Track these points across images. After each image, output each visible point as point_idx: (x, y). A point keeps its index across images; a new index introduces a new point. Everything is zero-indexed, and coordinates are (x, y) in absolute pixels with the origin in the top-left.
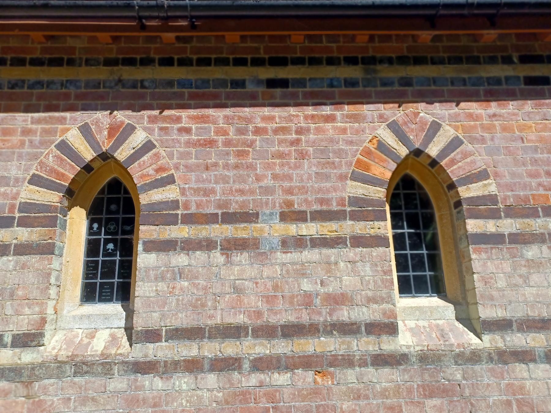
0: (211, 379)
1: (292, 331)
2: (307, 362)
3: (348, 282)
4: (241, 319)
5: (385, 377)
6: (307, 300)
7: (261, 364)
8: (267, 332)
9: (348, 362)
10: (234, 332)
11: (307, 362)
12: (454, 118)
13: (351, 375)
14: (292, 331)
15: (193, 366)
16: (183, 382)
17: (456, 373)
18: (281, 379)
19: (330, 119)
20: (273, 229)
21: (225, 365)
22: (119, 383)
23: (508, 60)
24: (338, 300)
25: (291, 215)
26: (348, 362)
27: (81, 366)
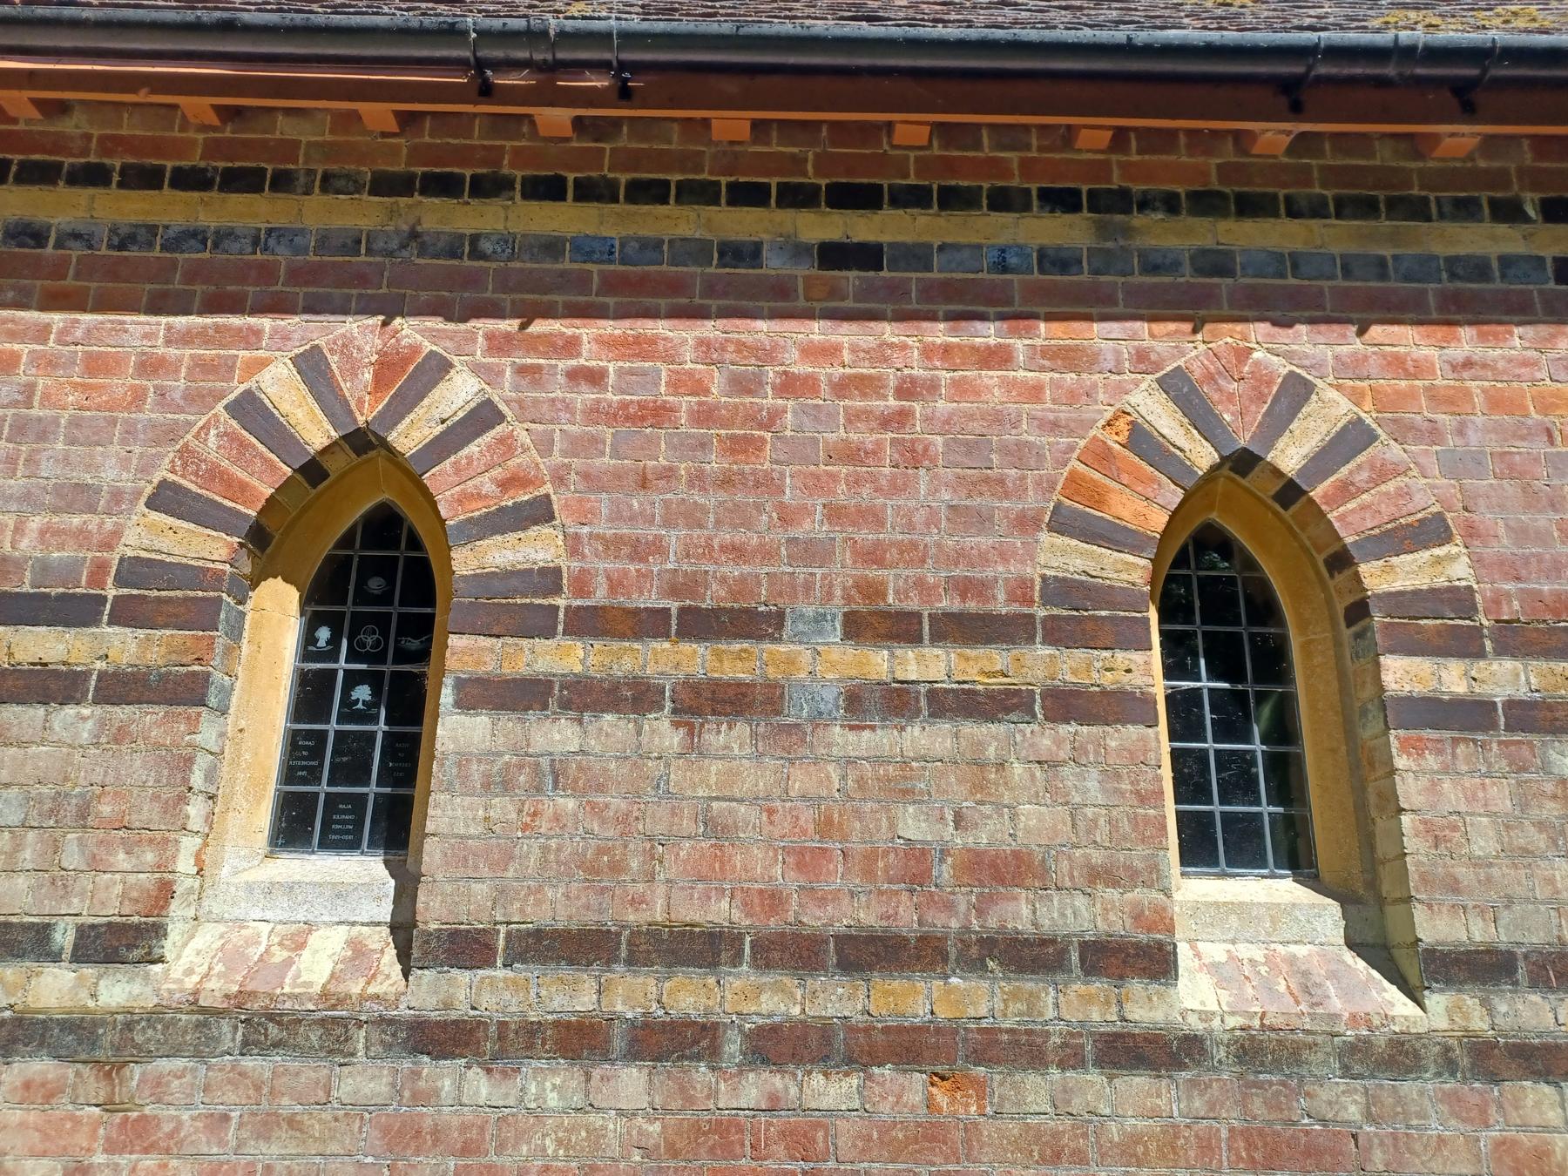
0: (631, 1083)
1: (867, 953)
2: (908, 1047)
3: (1032, 821)
4: (721, 912)
5: (1133, 1102)
6: (915, 867)
7: (776, 1046)
8: (796, 953)
9: (1027, 1050)
10: (702, 948)
11: (908, 1047)
12: (1351, 368)
13: (1034, 1091)
14: (867, 953)
15: (579, 1041)
16: (549, 1085)
17: (1344, 1100)
18: (830, 1091)
19: (996, 358)
20: (822, 661)
21: (669, 1042)
22: (366, 1080)
23: (1508, 212)
24: (1004, 870)
25: (874, 624)
26: (1027, 1050)
27: (264, 1025)
